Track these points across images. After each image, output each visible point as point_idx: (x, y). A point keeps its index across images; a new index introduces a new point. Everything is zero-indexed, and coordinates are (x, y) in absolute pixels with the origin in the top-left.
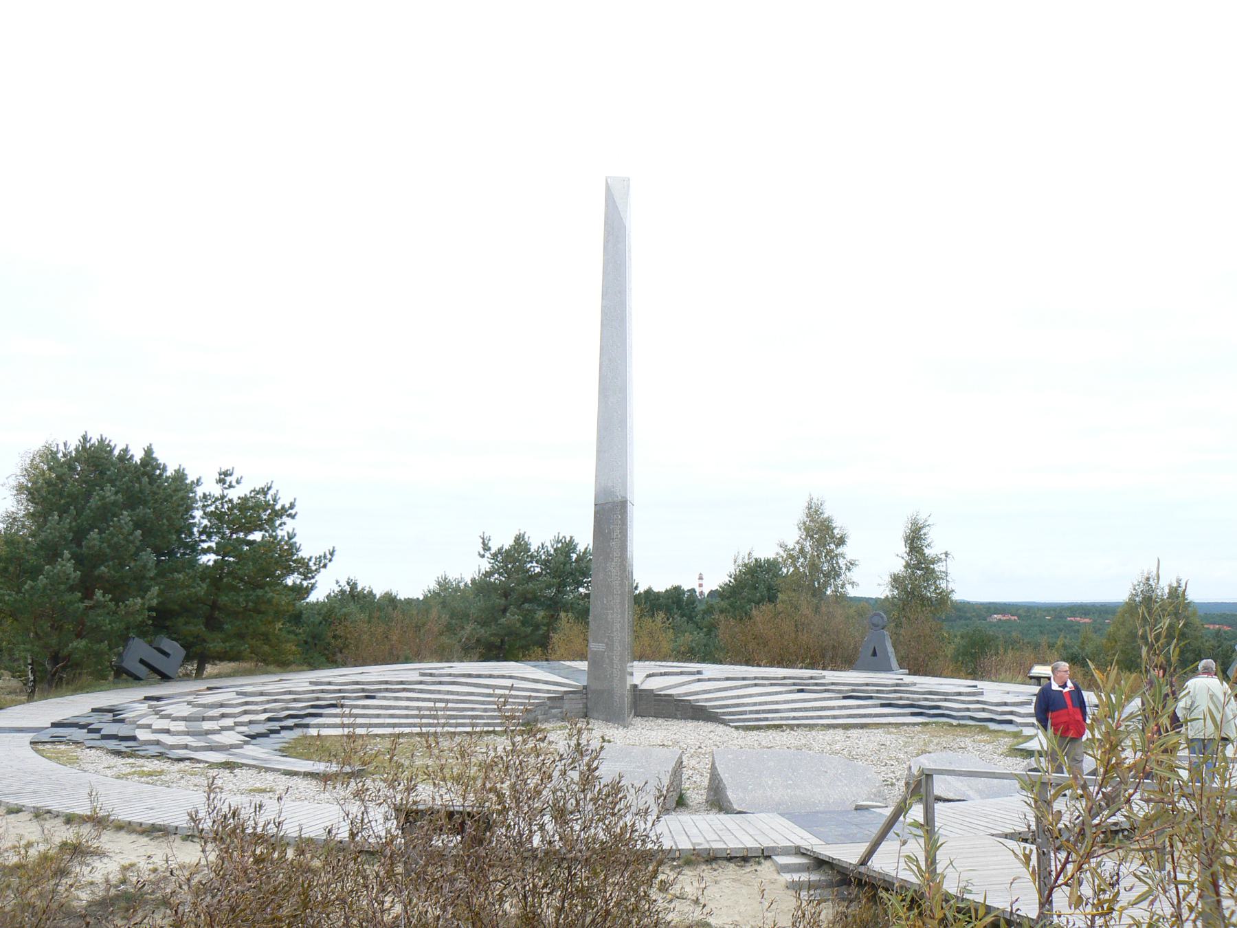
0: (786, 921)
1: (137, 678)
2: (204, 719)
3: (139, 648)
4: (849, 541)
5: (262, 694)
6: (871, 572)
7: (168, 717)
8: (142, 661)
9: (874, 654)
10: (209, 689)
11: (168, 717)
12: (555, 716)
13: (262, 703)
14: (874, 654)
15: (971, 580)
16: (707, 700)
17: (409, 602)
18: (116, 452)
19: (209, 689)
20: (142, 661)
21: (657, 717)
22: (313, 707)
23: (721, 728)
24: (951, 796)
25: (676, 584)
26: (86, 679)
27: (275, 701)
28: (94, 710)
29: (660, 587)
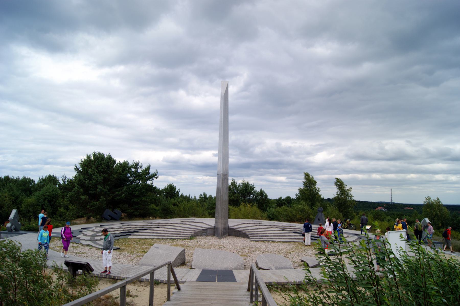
0: (288, 303)
1: (108, 220)
2: (96, 236)
3: (108, 212)
4: (206, 192)
6: (328, 192)
8: (109, 216)
10: (101, 226)
11: (86, 235)
12: (204, 235)
15: (358, 194)
16: (244, 230)
17: (187, 199)
18: (92, 158)
19: (101, 226)
20: (109, 216)
22: (122, 233)
23: (249, 240)
24: (265, 268)
27: (117, 230)
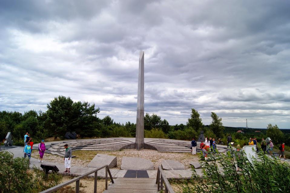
3: (68, 134)
5: (71, 144)
6: (207, 121)
7: (54, 148)
8: (69, 136)
9: (201, 138)
10: (64, 142)
11: (54, 148)
12: (129, 148)
13: (71, 146)
14: (201, 138)
15: (226, 122)
17: (118, 125)
21: (236, 128)
23: (157, 151)
24: (167, 169)
25: (181, 123)
26: (84, 138)
28: (51, 144)
29: (206, 125)
